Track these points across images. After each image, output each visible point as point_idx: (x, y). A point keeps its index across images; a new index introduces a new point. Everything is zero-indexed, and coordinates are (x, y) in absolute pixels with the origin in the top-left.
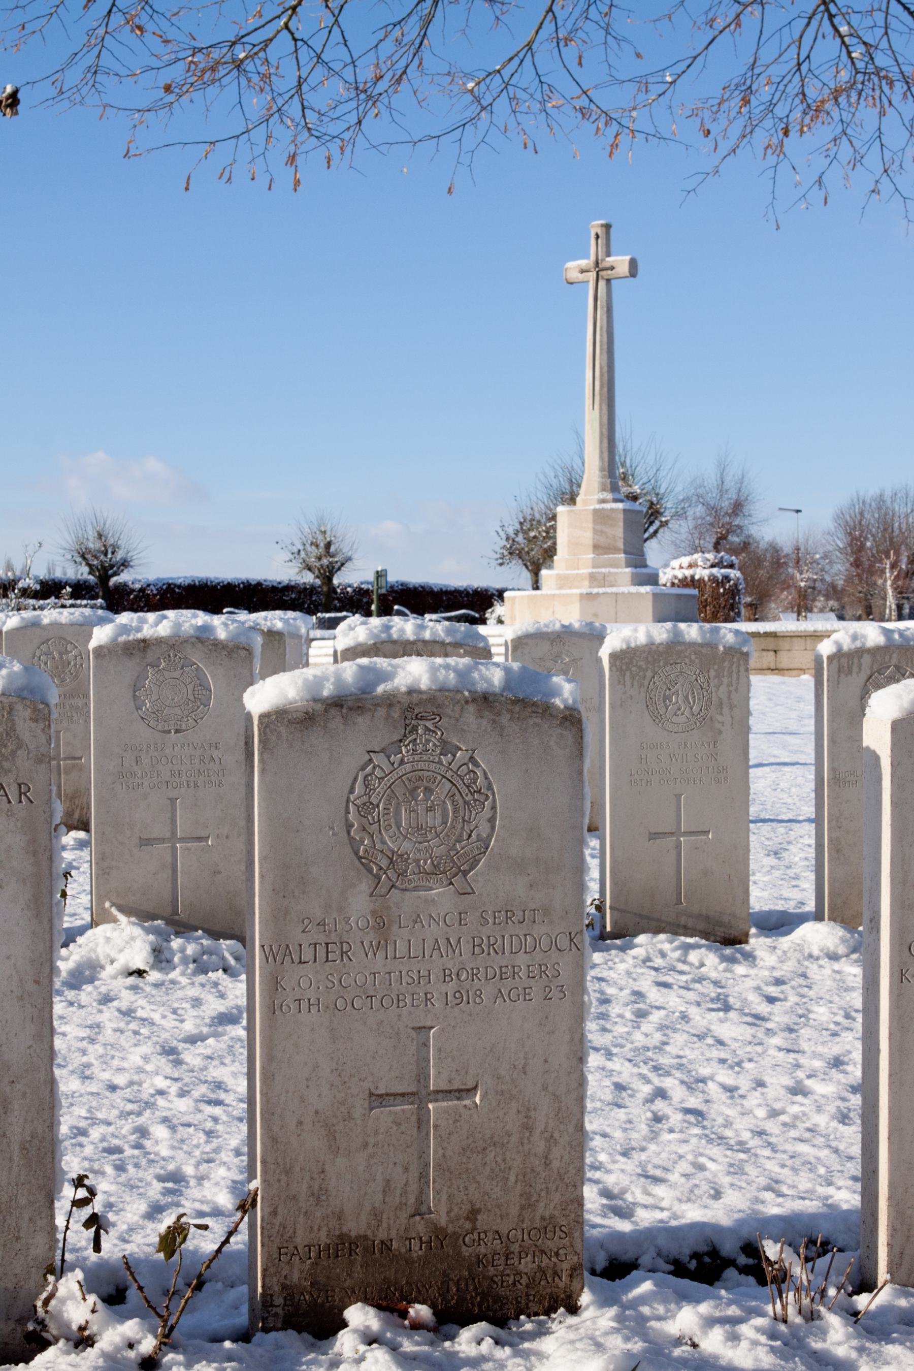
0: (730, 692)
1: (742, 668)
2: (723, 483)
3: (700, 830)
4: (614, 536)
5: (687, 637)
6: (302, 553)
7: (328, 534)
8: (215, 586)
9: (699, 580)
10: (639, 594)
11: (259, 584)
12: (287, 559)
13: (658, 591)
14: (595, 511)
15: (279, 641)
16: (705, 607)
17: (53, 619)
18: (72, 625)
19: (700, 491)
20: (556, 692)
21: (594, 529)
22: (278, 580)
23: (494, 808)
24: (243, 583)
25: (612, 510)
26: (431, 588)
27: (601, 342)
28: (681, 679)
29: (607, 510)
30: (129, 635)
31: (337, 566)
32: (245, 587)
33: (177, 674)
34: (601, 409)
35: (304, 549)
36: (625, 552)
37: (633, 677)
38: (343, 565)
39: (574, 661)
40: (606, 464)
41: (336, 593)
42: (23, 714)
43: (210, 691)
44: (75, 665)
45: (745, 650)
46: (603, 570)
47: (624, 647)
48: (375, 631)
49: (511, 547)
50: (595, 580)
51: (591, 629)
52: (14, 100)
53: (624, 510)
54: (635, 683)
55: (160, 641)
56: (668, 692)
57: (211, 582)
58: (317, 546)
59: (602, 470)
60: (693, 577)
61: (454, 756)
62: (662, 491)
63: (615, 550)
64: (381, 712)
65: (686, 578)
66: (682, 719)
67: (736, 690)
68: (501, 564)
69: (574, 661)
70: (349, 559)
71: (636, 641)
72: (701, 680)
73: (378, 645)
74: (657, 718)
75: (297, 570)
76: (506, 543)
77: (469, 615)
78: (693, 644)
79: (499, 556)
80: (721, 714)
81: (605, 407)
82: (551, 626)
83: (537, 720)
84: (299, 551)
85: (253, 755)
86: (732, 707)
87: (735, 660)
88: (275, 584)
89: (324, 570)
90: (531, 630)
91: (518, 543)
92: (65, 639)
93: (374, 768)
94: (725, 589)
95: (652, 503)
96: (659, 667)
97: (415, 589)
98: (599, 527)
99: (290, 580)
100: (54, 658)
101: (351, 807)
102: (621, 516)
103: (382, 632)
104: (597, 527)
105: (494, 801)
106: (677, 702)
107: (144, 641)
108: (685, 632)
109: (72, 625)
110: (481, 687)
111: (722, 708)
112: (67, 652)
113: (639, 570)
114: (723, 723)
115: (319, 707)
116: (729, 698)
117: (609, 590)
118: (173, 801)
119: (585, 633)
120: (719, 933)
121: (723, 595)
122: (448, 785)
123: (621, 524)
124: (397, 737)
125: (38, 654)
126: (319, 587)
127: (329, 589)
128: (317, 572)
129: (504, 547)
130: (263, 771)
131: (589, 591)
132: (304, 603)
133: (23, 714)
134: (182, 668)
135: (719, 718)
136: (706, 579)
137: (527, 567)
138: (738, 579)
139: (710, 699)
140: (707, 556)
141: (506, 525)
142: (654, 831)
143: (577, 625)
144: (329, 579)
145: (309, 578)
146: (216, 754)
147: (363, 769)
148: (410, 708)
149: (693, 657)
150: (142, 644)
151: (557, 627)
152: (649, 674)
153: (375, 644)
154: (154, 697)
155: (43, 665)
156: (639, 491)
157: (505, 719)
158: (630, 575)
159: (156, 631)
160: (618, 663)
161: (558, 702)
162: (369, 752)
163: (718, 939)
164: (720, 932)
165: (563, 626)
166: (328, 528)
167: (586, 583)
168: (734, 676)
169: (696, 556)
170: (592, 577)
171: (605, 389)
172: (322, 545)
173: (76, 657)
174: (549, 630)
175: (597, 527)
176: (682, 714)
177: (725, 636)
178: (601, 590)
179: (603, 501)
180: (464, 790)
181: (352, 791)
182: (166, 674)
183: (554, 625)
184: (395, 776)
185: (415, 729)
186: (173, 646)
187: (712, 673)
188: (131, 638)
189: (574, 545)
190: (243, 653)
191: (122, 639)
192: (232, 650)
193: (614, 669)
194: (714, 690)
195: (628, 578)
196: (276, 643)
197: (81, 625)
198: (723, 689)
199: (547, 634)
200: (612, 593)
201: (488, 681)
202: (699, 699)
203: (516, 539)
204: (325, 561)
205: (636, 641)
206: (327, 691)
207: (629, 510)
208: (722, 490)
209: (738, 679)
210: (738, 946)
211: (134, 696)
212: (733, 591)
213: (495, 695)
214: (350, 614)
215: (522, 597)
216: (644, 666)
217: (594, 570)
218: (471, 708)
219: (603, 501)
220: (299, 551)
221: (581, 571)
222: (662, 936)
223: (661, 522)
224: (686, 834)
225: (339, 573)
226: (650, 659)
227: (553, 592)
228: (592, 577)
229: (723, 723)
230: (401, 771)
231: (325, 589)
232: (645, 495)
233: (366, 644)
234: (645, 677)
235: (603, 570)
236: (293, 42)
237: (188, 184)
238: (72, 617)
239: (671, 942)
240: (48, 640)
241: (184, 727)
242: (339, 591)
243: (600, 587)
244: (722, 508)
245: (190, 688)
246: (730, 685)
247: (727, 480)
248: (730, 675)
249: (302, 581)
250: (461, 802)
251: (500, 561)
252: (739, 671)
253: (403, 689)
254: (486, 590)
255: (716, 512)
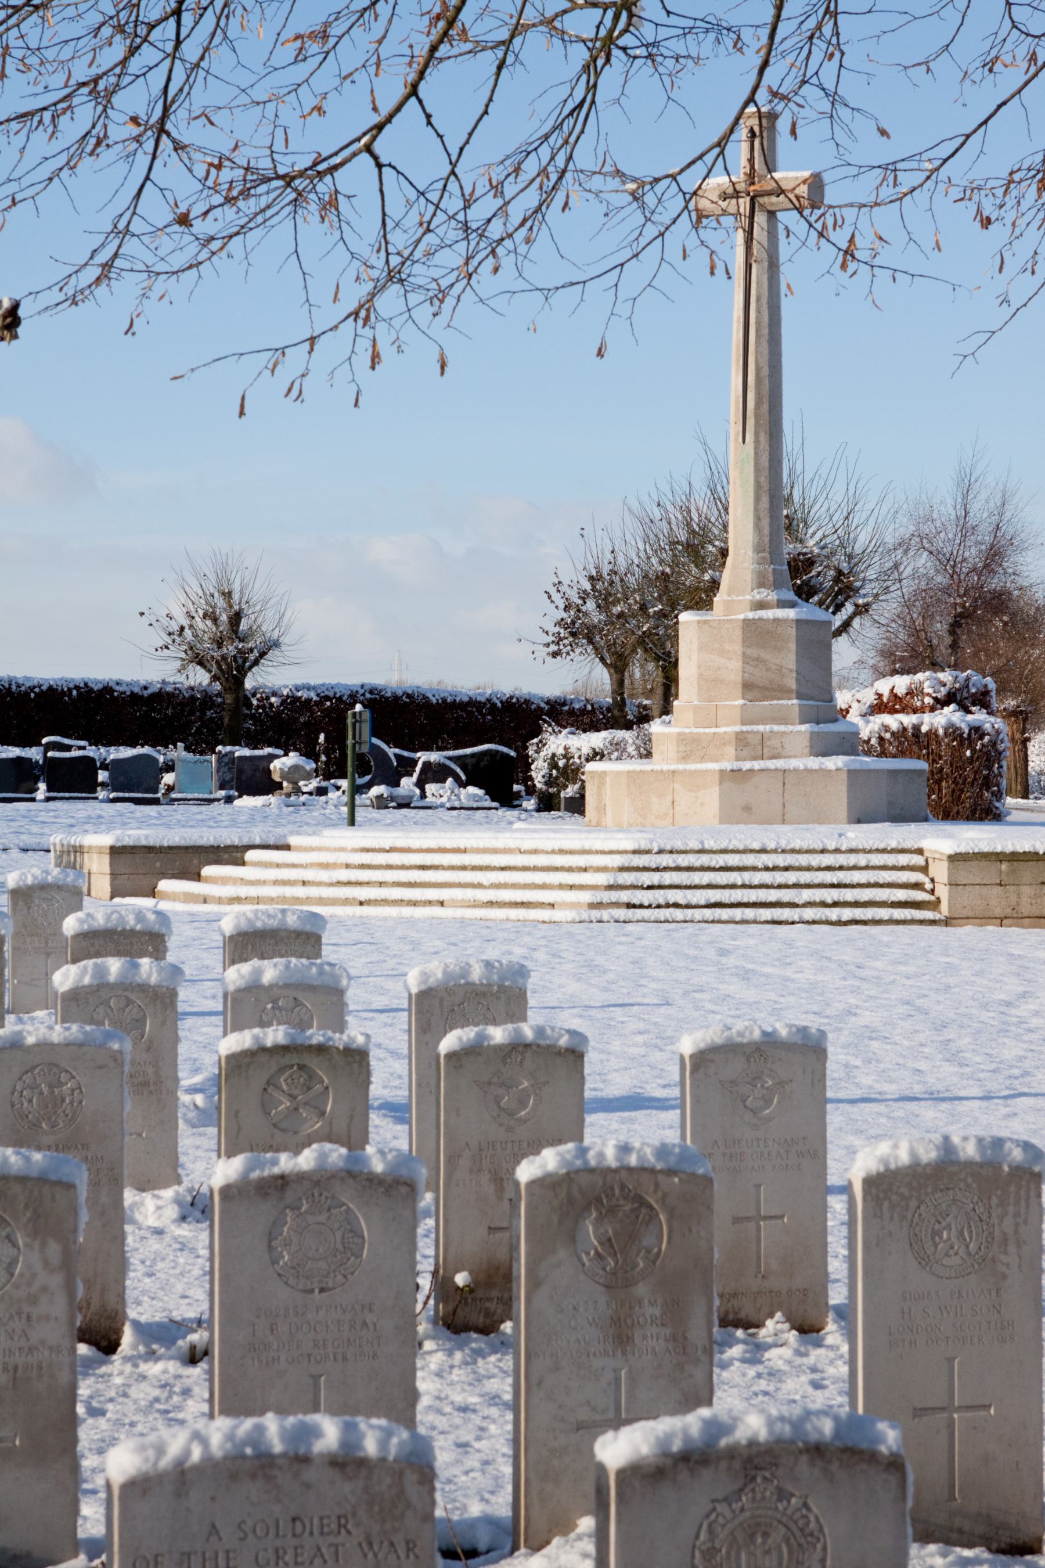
0: (1017, 1225)
1: (1032, 1193)
2: (966, 513)
3: (978, 1403)
4: (780, 668)
5: (961, 1154)
6: (188, 633)
7: (236, 597)
8: (27, 694)
9: (928, 734)
10: (823, 772)
11: (107, 689)
12: (161, 643)
13: (858, 766)
14: (746, 622)
15: (360, 1062)
16: (939, 782)
17: (41, 1037)
18: (67, 1045)
19: (925, 529)
20: (880, 1438)
21: (744, 654)
22: (143, 683)
23: (825, 1549)
24: (77, 687)
25: (776, 621)
26: (425, 697)
27: (758, 323)
28: (954, 1209)
29: (767, 620)
30: (263, 1170)
31: (252, 657)
32: (79, 694)
33: (322, 1218)
34: (757, 442)
35: (191, 626)
36: (799, 697)
37: (893, 1207)
38: (262, 655)
39: (781, 1084)
40: (767, 539)
41: (249, 705)
42: (411, 1478)
43: (363, 1238)
44: (72, 1102)
45: (1037, 1169)
46: (761, 728)
47: (882, 1169)
48: (568, 1157)
49: (573, 623)
50: (747, 745)
51: (804, 1037)
52: (12, 320)
53: (798, 622)
54: (896, 1215)
55: (302, 1177)
56: (937, 1226)
57: (18, 686)
58: (215, 620)
59: (758, 549)
60: (917, 728)
61: (789, 1502)
62: (858, 549)
63: (782, 692)
64: (723, 1465)
65: (905, 729)
66: (955, 1261)
67: (1026, 1222)
68: (555, 654)
69: (781, 1084)
70: (276, 644)
71: (896, 1162)
72: (980, 1210)
73: (572, 1175)
74: (924, 1260)
75: (178, 664)
76: (565, 615)
77: (497, 751)
78: (969, 1164)
79: (551, 638)
80: (1006, 1253)
81: (763, 438)
82: (747, 1034)
83: (864, 1467)
84: (182, 629)
85: (608, 1505)
86: (1019, 1244)
87: (1024, 1183)
88: (136, 690)
89: (229, 666)
90: (719, 1040)
91: (586, 614)
92: (57, 1066)
93: (718, 1516)
94: (974, 751)
95: (840, 573)
96: (927, 1194)
97: (396, 698)
98: (753, 652)
99: (164, 682)
100: (41, 1093)
101: (697, 1554)
102: (792, 632)
103: (577, 1157)
104: (749, 652)
105: (825, 1543)
106: (949, 1239)
107: (282, 1177)
108: (960, 1149)
109: (68, 1045)
110: (814, 1437)
111: (1006, 1245)
112: (60, 1084)
113: (824, 727)
114: (1008, 1265)
115: (669, 1462)
116: (1016, 1232)
117: (771, 764)
118: (316, 1378)
119: (795, 1044)
120: (1003, 1539)
121: (971, 760)
122: (783, 1530)
123: (793, 646)
124: (736, 1487)
125: (19, 1087)
126: (219, 695)
127: (237, 700)
128: (214, 669)
129: (560, 623)
130: (619, 1521)
131: (736, 765)
132: (189, 724)
133: (411, 1478)
134: (329, 1210)
135: (1003, 1257)
136: (941, 732)
137: (602, 660)
138: (998, 732)
139: (991, 1234)
140: (941, 676)
141: (566, 581)
142: (919, 1406)
143: (784, 1032)
144: (239, 682)
145: (199, 678)
146: (370, 1318)
147: (707, 1516)
148: (750, 1459)
149: (970, 1180)
150: (280, 1182)
151: (757, 1035)
152: (913, 1203)
153: (568, 1174)
154: (294, 1248)
155: (26, 1104)
156: (816, 551)
157: (835, 1467)
158: (808, 736)
159: (296, 1164)
160: (873, 1190)
161: (883, 1449)
162: (713, 1501)
163: (1003, 1546)
164: (1005, 1540)
165: (765, 1034)
166: (236, 587)
167: (731, 751)
168: (1023, 1203)
169: (920, 676)
170: (741, 740)
171: (765, 407)
172: (224, 618)
173: (73, 1090)
174: (745, 1041)
175: (749, 652)
176: (956, 1254)
177: (1010, 1151)
178: (757, 765)
179: (761, 605)
180: (798, 1533)
181: (697, 1536)
182: (310, 1219)
183: (751, 1033)
184: (736, 1522)
185: (754, 1478)
186: (317, 1183)
187: (995, 1201)
188: (266, 1173)
189: (709, 682)
190: (404, 1190)
191: (255, 1175)
192: (390, 1186)
193: (869, 1198)
194: (996, 1221)
195: (804, 743)
196: (356, 1066)
197: (81, 1045)
198: (1008, 1224)
199: (740, 1045)
200: (776, 770)
201: (820, 1432)
202: (977, 1235)
203: (584, 608)
204: (230, 649)
205: (896, 1162)
206: (676, 1446)
207: (807, 622)
208: (965, 529)
209: (1028, 1207)
210: (1028, 1557)
211: (270, 1247)
212: (988, 753)
213: (826, 1445)
214: (280, 752)
215: (618, 774)
216: (907, 1194)
217: (745, 728)
218: (804, 1458)
219: (761, 605)
220: (182, 629)
221: (722, 730)
222: (932, 1548)
223: (857, 606)
224: (960, 1409)
225: (255, 669)
226: (914, 1184)
227: (673, 767)
228: (741, 740)
229: (1008, 1265)
230: (741, 1518)
231: (229, 699)
232: (827, 557)
233: (556, 1174)
234: (907, 1207)
235: (761, 728)
236: (376, 170)
237: (242, 406)
238: (67, 1033)
239: (944, 1555)
240: (34, 1067)
241: (330, 1285)
242: (255, 702)
243: (755, 758)
244: (964, 560)
245: (339, 1235)
246: (1017, 1215)
247: (975, 508)
248: (1017, 1203)
249: (187, 684)
250: (795, 1546)
251: (553, 648)
252: (1028, 1197)
253: (744, 1442)
254: (527, 702)
255: (953, 567)
